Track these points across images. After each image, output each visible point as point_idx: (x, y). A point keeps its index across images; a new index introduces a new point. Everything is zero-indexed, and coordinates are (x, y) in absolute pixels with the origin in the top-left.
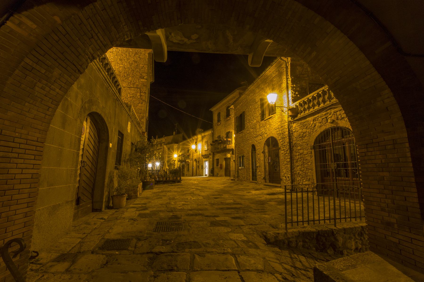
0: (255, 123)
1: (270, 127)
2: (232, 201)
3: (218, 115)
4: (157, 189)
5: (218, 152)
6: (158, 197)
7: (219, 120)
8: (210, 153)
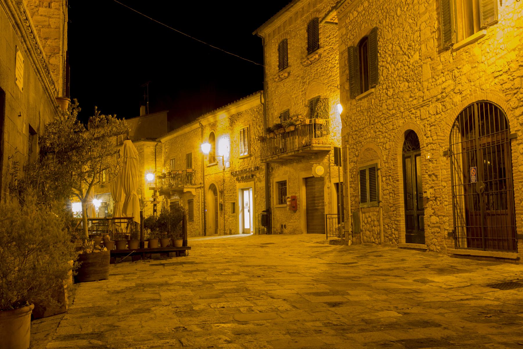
0: (417, 62)
1: (473, 71)
2: (394, 314)
3: (279, 50)
4: (118, 278)
5: (284, 162)
6: (136, 306)
7: (283, 64)
8: (258, 162)
